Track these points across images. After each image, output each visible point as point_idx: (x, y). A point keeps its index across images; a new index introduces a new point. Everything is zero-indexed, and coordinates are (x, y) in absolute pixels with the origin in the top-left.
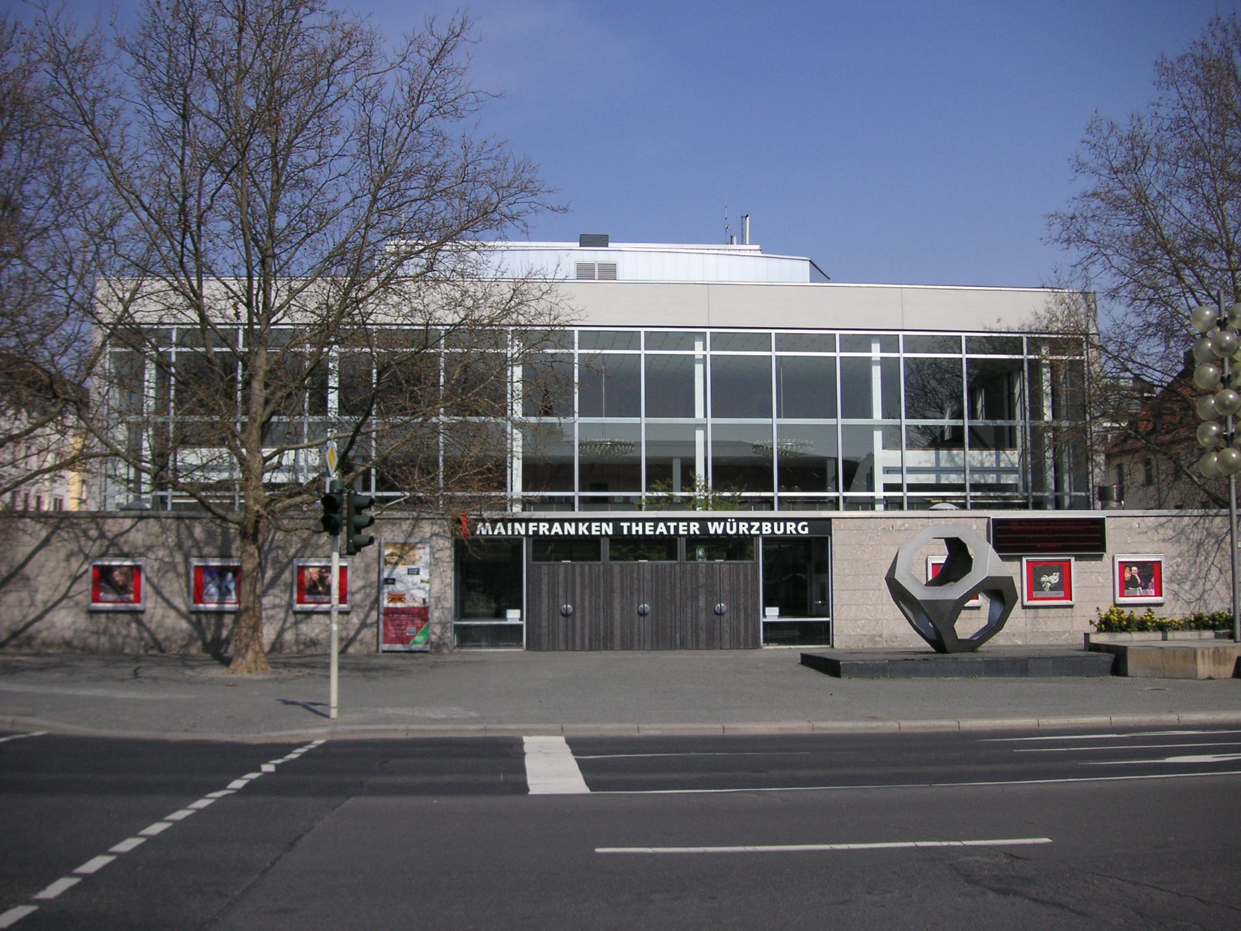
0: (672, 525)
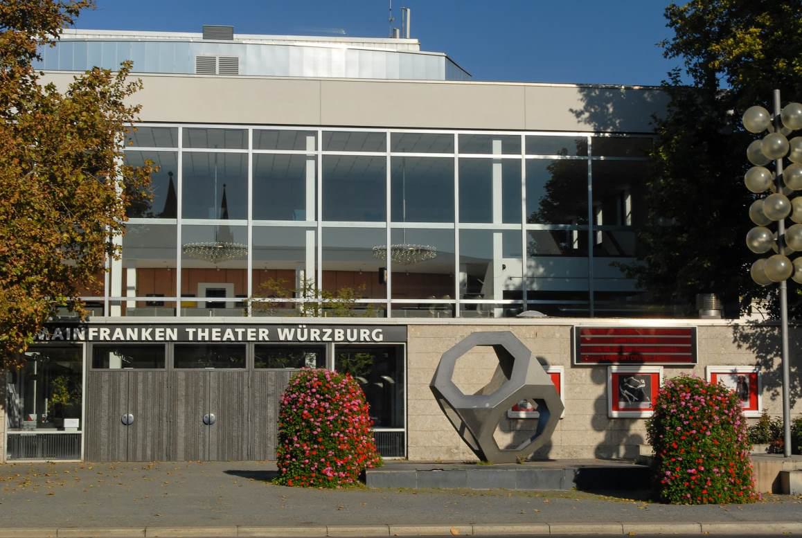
0: (240, 331)
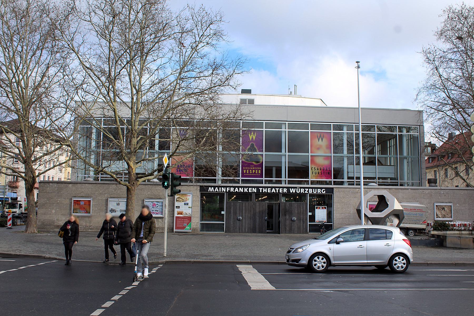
0: (277, 189)
